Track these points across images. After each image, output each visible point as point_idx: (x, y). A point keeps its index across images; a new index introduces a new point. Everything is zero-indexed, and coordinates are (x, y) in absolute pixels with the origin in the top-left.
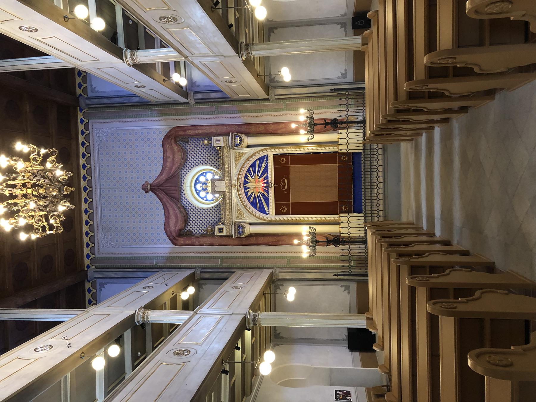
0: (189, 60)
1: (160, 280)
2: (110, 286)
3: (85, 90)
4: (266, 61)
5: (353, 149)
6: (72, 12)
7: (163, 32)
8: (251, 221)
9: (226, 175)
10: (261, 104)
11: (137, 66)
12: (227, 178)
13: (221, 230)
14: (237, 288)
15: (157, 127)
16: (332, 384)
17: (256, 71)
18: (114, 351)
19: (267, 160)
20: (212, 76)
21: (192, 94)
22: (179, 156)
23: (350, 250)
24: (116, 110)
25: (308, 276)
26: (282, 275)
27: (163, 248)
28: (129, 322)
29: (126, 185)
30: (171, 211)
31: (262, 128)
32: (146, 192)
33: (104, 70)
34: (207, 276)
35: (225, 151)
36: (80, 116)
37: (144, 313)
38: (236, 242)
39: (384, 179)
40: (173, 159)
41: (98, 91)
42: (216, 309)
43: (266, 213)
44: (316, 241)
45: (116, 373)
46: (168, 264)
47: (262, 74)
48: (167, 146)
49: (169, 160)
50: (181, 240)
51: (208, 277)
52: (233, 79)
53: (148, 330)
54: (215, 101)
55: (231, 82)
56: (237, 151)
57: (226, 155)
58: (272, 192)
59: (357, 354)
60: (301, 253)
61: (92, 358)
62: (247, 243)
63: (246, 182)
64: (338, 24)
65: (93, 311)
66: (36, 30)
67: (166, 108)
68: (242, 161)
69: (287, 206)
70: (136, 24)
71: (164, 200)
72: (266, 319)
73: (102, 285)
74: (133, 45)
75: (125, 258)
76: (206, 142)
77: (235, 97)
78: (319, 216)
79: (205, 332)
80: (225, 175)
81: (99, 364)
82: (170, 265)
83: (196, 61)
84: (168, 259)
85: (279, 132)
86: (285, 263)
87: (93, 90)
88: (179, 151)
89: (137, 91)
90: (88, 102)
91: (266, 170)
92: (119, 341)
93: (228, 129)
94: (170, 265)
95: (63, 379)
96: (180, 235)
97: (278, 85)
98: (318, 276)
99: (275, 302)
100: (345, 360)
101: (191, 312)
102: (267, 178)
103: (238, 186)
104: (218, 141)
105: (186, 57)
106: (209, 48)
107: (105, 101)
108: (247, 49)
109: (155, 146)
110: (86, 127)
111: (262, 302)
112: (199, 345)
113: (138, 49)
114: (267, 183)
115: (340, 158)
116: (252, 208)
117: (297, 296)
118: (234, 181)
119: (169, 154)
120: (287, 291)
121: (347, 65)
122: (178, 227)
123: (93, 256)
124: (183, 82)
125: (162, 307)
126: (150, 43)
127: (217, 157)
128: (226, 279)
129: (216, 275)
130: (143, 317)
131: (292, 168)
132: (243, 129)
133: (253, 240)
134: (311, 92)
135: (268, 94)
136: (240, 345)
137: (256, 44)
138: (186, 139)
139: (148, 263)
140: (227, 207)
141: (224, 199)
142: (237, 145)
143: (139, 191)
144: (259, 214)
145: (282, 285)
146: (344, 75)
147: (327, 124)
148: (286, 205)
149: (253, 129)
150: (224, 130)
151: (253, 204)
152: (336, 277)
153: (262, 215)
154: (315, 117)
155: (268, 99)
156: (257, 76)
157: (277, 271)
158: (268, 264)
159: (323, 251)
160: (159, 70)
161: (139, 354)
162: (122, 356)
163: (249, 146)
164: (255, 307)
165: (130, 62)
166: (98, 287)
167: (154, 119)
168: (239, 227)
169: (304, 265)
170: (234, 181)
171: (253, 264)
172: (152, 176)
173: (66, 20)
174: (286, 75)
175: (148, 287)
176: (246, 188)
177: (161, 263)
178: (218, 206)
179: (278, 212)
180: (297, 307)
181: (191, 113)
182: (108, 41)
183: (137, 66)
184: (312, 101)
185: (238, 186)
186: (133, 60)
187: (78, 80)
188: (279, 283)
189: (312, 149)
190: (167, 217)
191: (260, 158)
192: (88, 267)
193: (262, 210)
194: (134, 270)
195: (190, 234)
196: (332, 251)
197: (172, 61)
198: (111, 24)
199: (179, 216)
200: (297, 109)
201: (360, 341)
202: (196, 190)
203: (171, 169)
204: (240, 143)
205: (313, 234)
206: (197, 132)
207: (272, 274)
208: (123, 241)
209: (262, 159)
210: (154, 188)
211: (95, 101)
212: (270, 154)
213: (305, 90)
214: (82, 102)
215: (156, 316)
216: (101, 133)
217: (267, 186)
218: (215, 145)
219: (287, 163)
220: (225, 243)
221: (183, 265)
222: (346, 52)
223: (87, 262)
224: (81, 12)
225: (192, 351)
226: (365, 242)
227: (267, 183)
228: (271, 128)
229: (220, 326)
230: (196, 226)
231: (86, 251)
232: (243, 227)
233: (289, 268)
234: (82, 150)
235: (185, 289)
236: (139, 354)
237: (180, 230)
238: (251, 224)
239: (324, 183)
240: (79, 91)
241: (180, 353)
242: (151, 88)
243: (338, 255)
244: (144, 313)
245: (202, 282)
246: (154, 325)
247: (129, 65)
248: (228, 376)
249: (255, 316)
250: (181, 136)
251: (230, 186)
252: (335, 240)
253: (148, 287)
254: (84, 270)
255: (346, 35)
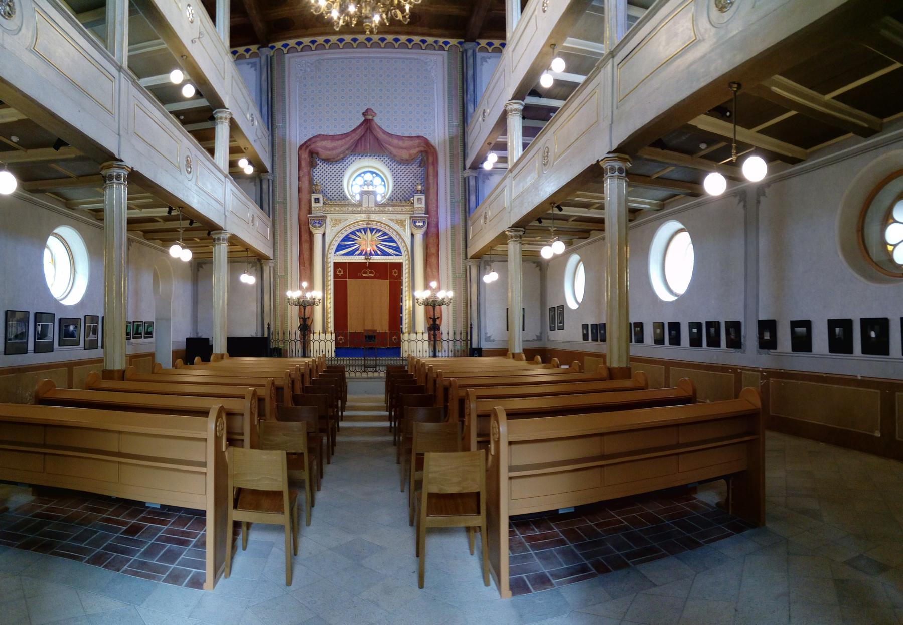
0: (508, 174)
1: (260, 134)
2: (252, 74)
3: (483, 49)
4: (503, 258)
5: (405, 346)
6: (560, 55)
7: (536, 149)
8: (329, 234)
9: (381, 208)
10: (462, 251)
11: (505, 115)
12: (377, 209)
13: (317, 200)
14: (253, 221)
15: (438, 130)
16: (156, 319)
17: (496, 245)
18: (189, 91)
19: (396, 255)
20: (492, 198)
21: (475, 174)
22: (405, 154)
23: (296, 341)
24: (459, 82)
25: (266, 298)
26: (267, 270)
27: (296, 133)
28: (218, 104)
29: (373, 90)
30: (339, 143)
31: (433, 250)
32: (364, 114)
33: (502, 77)
34: (265, 186)
35: (408, 209)
36: (453, 41)
37: (226, 118)
38: (303, 218)
39: (371, 378)
40: (401, 148)
41: (482, 64)
42: (229, 198)
43: (336, 251)
44: (304, 306)
45: (165, 95)
46: (277, 140)
47: (493, 252)
48: (417, 142)
49: (401, 144)
50: (305, 155)
51: (261, 186)
52: (488, 220)
53: (207, 125)
54: (466, 200)
55: (485, 218)
56: (408, 223)
57: (404, 209)
58: (360, 259)
59: (183, 346)
60: (292, 290)
61: (181, 69)
62: (303, 233)
63: (372, 230)
64: (541, 333)
65: (228, 60)
66: (544, 11)
67: (460, 144)
68: (397, 227)
69: (344, 276)
70: (546, 118)
71: (353, 135)
72: (221, 251)
73: (254, 65)
74: (528, 113)
75: (284, 89)
76: (420, 187)
77: (469, 223)
78: (332, 310)
79: (209, 188)
80: (382, 208)
81: (176, 76)
82: (275, 144)
83: (507, 181)
84: (284, 140)
85: (429, 269)
86: (280, 273)
87: (484, 59)
88: (410, 155)
89: (480, 111)
90: (470, 52)
91: (384, 253)
92: (198, 94)
93: (433, 213)
94: (275, 144)
95: (161, 40)
96: (311, 154)
97: (482, 268)
98: (267, 309)
99: (238, 262)
100: (177, 332)
101: (227, 171)
102: (376, 254)
103: (368, 221)
104: (419, 201)
105: (511, 171)
106: (518, 196)
107: (470, 73)
108: (516, 237)
109: (418, 127)
110: (442, 48)
111: (239, 248)
112: (196, 182)
113: (524, 118)
114: (371, 254)
115: (395, 334)
116: (342, 237)
117: (246, 285)
118: (374, 217)
119: (408, 143)
120: (251, 274)
121: (499, 341)
122: (320, 151)
123: (286, 51)
124: (488, 165)
125: (232, 138)
126: (529, 132)
127: (401, 199)
128: (262, 207)
129: (265, 197)
130: (221, 118)
131: (386, 282)
132: (433, 230)
133: (305, 237)
134: (470, 305)
135: (472, 258)
136: (194, 225)
137: (520, 248)
138: (423, 163)
139: (278, 117)
140: (344, 208)
141: (354, 205)
142: (415, 222)
143: (365, 105)
144: (336, 244)
145: (256, 270)
146: (488, 339)
147: (434, 320)
148: (346, 274)
149: (432, 240)
150: (432, 208)
151: (347, 238)
152: (266, 326)
153: (334, 247)
154: (444, 307)
155: (466, 258)
156: (490, 247)
157: (271, 264)
158: (278, 253)
159: (294, 314)
160: (500, 139)
161: (182, 118)
162: (184, 99)
163: (412, 235)
164: (234, 240)
165: (509, 108)
166: (253, 60)
167: (447, 128)
168: (321, 221)
169: (279, 293)
170: (374, 217)
171: (278, 237)
172: (380, 121)
173: (552, 46)
174: (491, 278)
175: (253, 121)
176: (365, 230)
177: (278, 133)
178: (345, 198)
179: (337, 265)
180: (235, 286)
181: (452, 172)
182: (529, 88)
183: (505, 115)
184: (462, 305)
185: (368, 221)
186: (511, 111)
187: (497, 43)
188: (258, 266)
189: (407, 304)
190: (333, 138)
191: (398, 248)
192: (273, 47)
193: (340, 248)
194: (270, 104)
195: (312, 165)
196: (294, 323)
197: (508, 154)
198: (548, 94)
199: (334, 152)
200: (454, 290)
201: (197, 349)
202: (364, 173)
203: (390, 145)
204: (416, 226)
205: (312, 303)
206: (431, 177)
207: (267, 259)
208: (305, 86)
209: (397, 249)
210: (367, 124)
211: (471, 61)
212: (403, 259)
213: (474, 298)
214: (469, 45)
215: (222, 133)
216: (434, 63)
217: (368, 255)
218: (416, 197)
219: (392, 277)
220: (303, 206)
221: (276, 158)
222: (507, 341)
223: (279, 45)
224: (559, 65)
225: (190, 176)
226: (304, 355)
227: (371, 254)
228: (433, 260)
229: (213, 202)
230: (321, 171)
231: (292, 42)
232: (321, 226)
233: (274, 277)
234: (417, 39)
235: (250, 162)
236: (182, 118)
237: (317, 154)
238: (324, 235)
239: (369, 315)
240: (483, 42)
241: (188, 164)
242: (482, 128)
243: (289, 329)
244: (226, 118)
245: (258, 181)
246: (213, 130)
247: (506, 106)
248: (166, 214)
249: (224, 240)
250: (428, 158)
251: (368, 212)
252: (306, 327)
253: (253, 121)
254: (269, 42)
255: (523, 341)
